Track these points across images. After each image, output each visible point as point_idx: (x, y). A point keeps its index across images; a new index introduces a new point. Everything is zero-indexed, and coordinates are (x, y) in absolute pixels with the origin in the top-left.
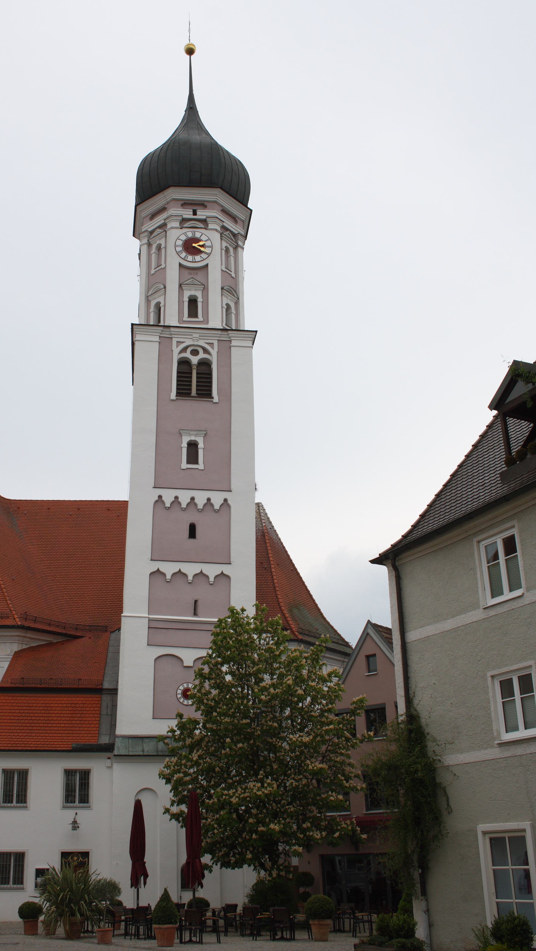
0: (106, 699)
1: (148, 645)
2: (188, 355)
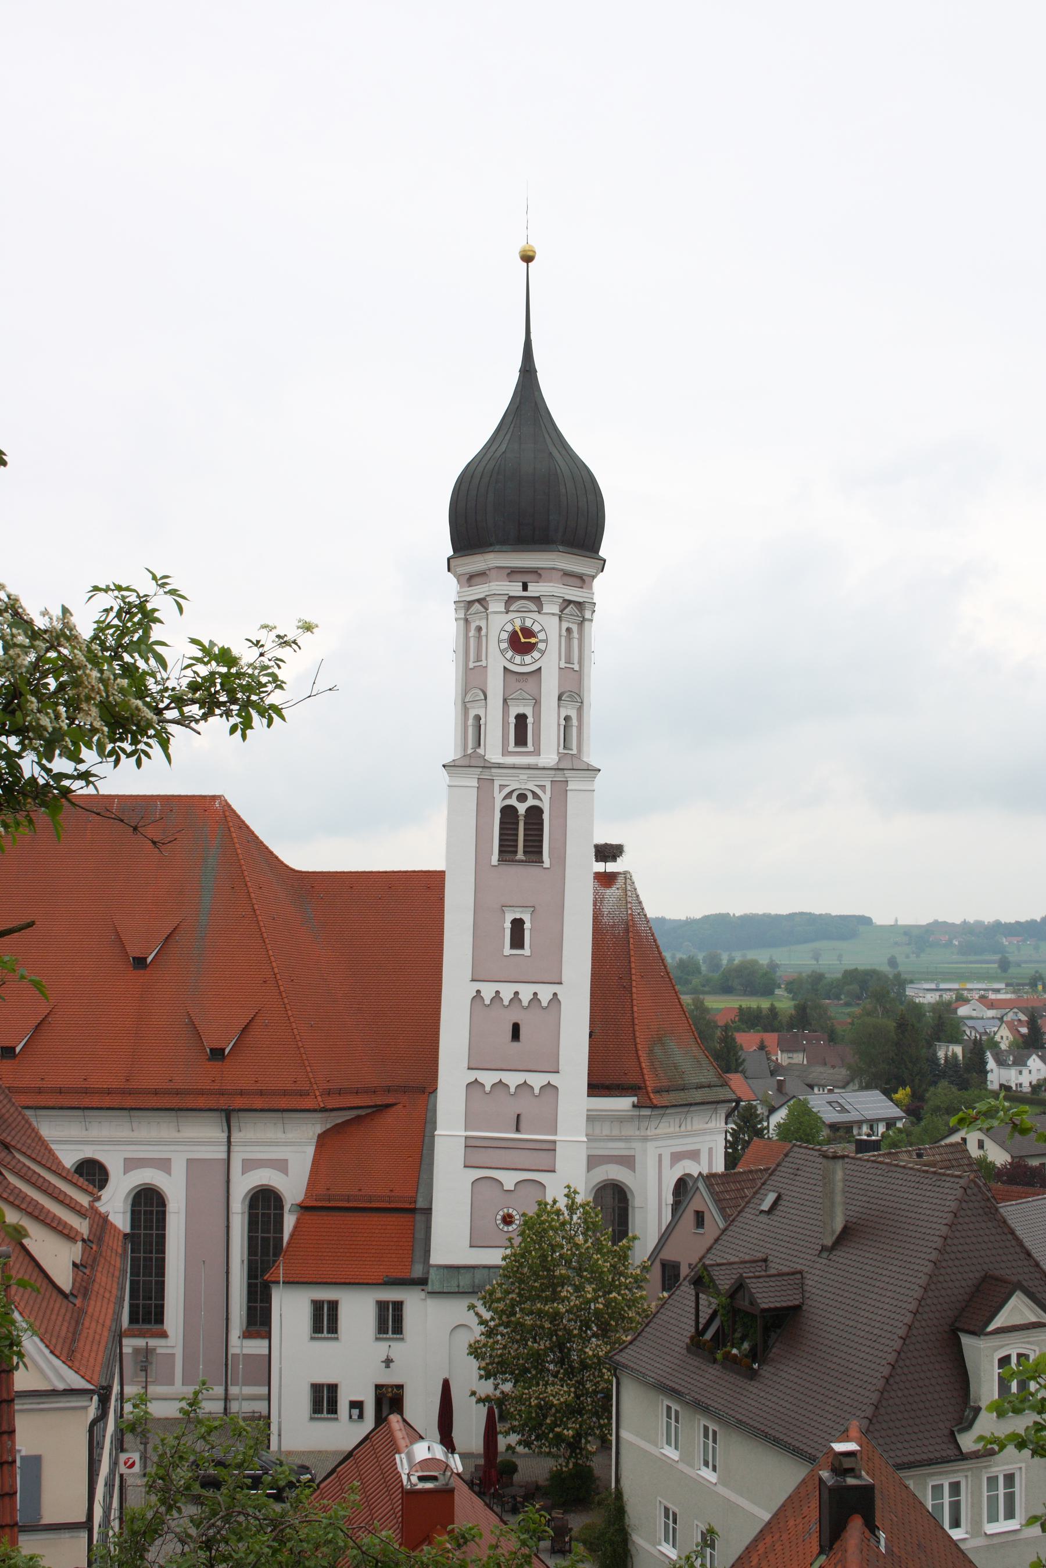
0: (419, 1217)
1: (465, 1167)
2: (513, 801)
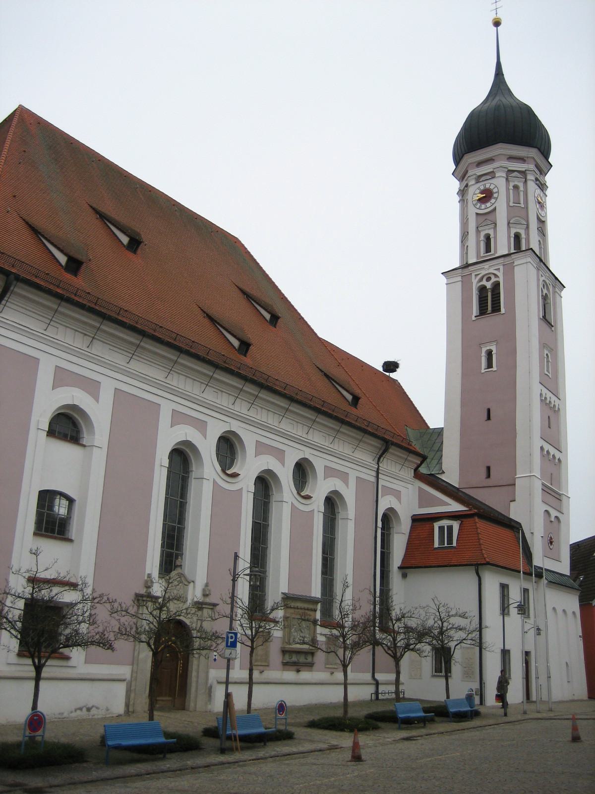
2: (484, 282)
